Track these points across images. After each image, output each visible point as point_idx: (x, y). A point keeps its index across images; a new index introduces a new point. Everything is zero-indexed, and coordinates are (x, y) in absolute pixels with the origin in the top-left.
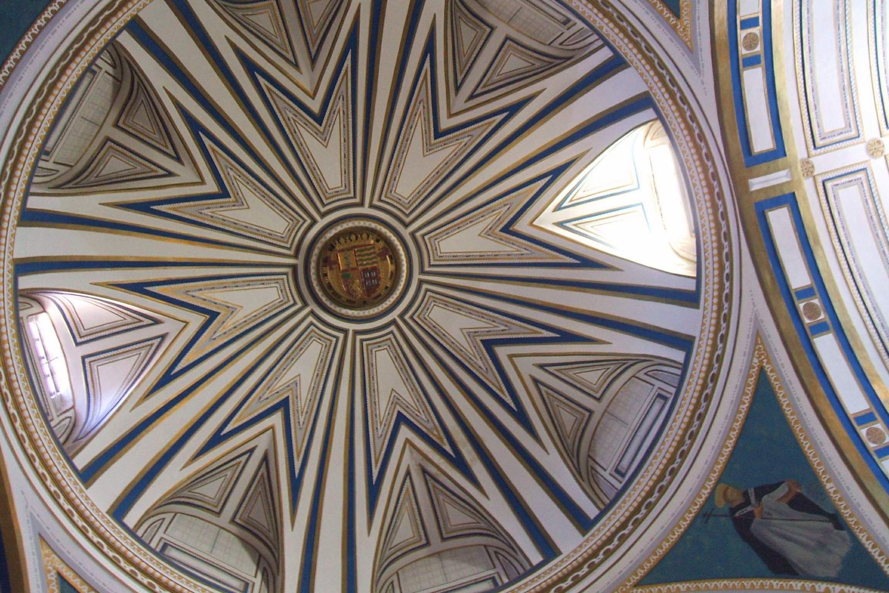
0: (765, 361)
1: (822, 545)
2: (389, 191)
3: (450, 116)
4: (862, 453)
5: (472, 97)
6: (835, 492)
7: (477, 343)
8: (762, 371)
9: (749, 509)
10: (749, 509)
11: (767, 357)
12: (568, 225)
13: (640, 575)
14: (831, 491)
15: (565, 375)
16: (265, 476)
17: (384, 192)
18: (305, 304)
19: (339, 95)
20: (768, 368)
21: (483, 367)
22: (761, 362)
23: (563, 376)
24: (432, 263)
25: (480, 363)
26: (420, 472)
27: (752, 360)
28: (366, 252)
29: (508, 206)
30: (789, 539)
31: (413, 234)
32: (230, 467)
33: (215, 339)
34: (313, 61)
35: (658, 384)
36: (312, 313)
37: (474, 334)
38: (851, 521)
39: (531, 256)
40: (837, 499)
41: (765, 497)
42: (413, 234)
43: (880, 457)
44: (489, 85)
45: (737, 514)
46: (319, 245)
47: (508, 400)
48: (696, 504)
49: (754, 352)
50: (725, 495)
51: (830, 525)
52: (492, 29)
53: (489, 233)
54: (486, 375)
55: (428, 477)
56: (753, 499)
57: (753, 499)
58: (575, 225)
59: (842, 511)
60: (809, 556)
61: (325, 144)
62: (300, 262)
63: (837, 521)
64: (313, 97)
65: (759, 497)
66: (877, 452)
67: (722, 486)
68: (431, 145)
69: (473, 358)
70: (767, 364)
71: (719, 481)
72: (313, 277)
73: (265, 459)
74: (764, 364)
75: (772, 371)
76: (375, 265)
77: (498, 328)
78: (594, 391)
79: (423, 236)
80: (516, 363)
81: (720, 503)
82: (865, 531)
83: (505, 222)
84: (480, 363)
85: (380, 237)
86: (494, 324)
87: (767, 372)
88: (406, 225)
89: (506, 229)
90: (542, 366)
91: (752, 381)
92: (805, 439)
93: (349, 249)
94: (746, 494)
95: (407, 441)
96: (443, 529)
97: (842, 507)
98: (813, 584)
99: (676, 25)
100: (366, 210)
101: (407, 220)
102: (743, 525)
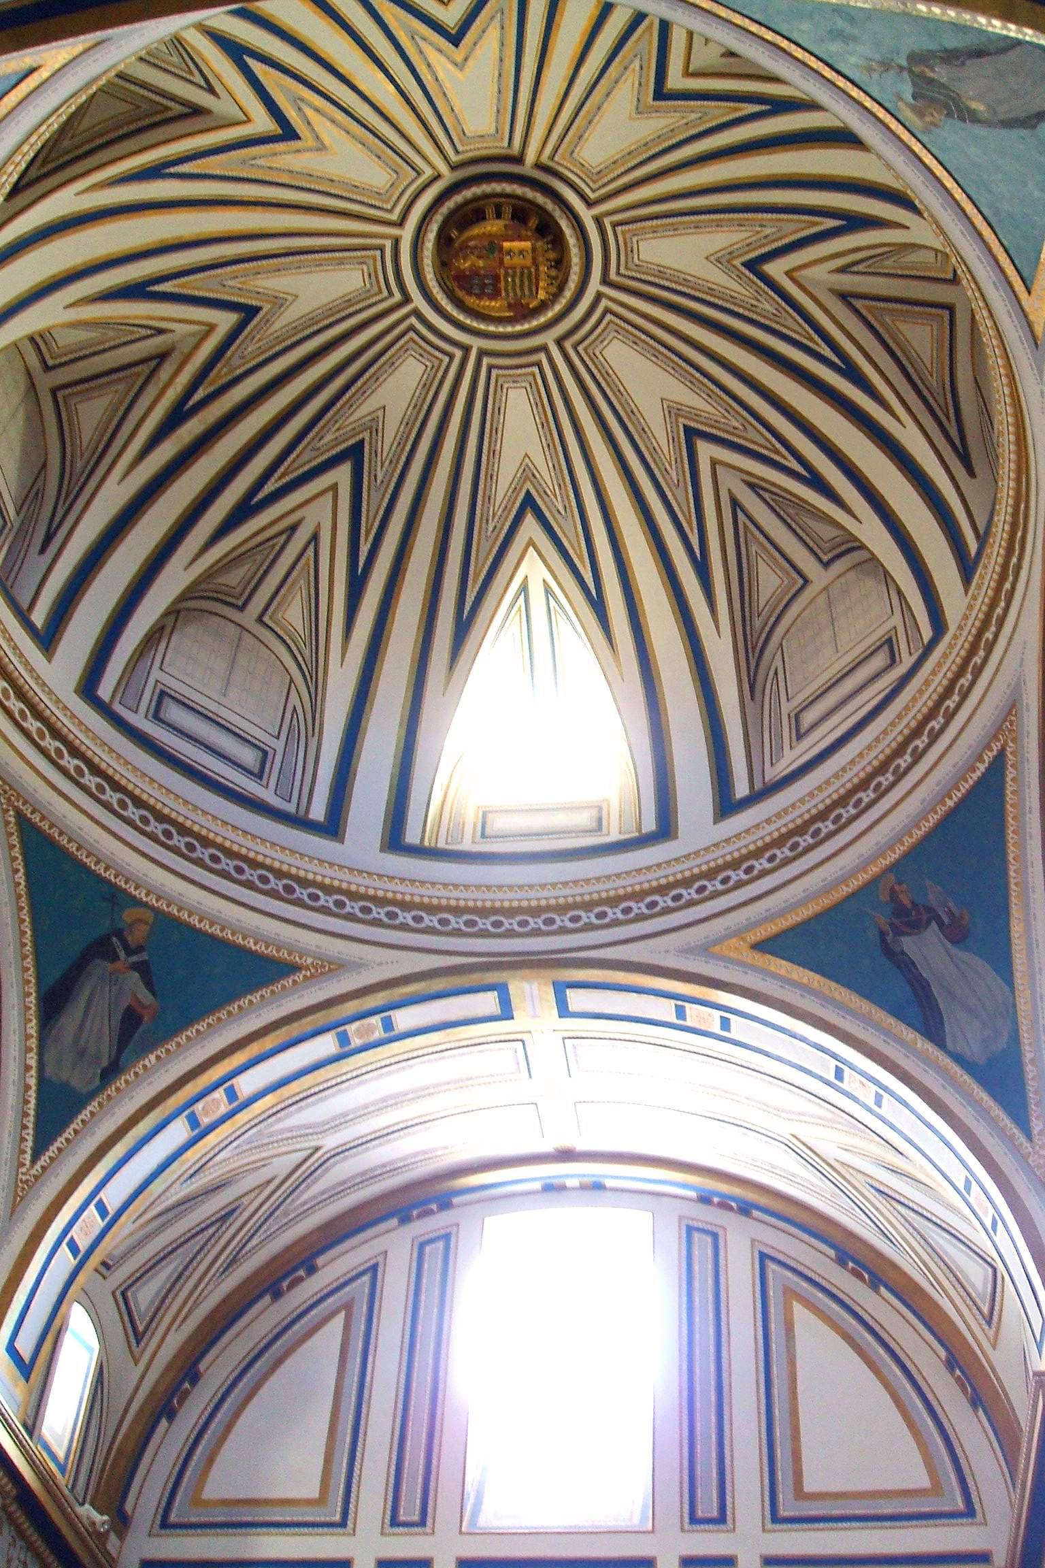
0: (308, 974)
1: (82, 1053)
2: (618, 329)
3: (714, 463)
4: (192, 1098)
5: (735, 504)
6: (145, 1067)
7: (358, 434)
8: (295, 968)
9: (122, 954)
10: (122, 954)
11: (312, 976)
12: (522, 598)
13: (33, 817)
14: (147, 1062)
15: (300, 573)
16: (169, 114)
17: (618, 321)
18: (453, 168)
19: (783, 313)
20: (299, 977)
21: (322, 442)
22: (307, 968)
23: (298, 567)
24: (494, 372)
25: (329, 437)
26: (163, 349)
27: (310, 956)
28: (526, 283)
29: (563, 512)
30: (87, 1009)
31: (544, 348)
32: (184, 60)
33: (413, 38)
34: (845, 297)
35: (279, 745)
36: (438, 177)
37: (374, 426)
38: (111, 1091)
39: (483, 536)
40: (137, 1070)
41: (137, 974)
42: (544, 348)
43: (187, 1117)
44: (745, 533)
45: (114, 939)
46: (549, 205)
47: (269, 487)
48: (126, 883)
49: (320, 959)
50: (140, 920)
51: (105, 1063)
52: (826, 565)
53: (527, 472)
54: (310, 447)
55: (153, 364)
56: (134, 959)
57: (134, 959)
58: (520, 609)
59: (123, 1078)
60: (68, 1037)
61: (712, 258)
62: (527, 168)
63: (111, 1072)
64: (788, 274)
65: (136, 967)
66: (193, 1114)
67: (149, 916)
68: (677, 415)
69: (337, 426)
70: (304, 976)
71: (156, 911)
72: (497, 187)
73: (197, 111)
74: (304, 972)
75: (294, 981)
76: (503, 294)
77: (379, 470)
78: (273, 614)
79: (539, 365)
80: (321, 499)
81: (129, 915)
82: (101, 1108)
83: (539, 502)
84: (329, 437)
85: (544, 306)
86: (388, 462)
87: (294, 974)
88: (559, 342)
89: (529, 501)
90: (315, 538)
91: (284, 955)
92: (209, 1024)
93: (534, 260)
94: (140, 949)
95: (212, 328)
96: (70, 390)
97: (128, 1077)
98: (35, 1050)
99: (744, 939)
100: (594, 285)
101: (568, 345)
102: (101, 949)
